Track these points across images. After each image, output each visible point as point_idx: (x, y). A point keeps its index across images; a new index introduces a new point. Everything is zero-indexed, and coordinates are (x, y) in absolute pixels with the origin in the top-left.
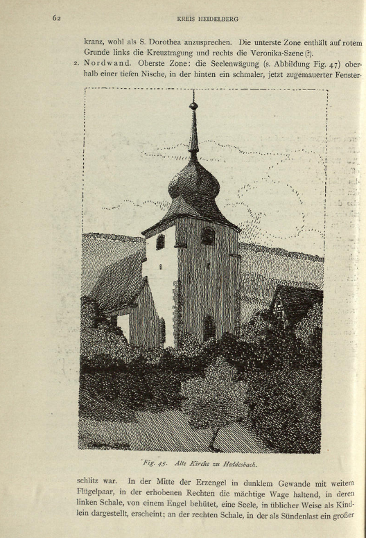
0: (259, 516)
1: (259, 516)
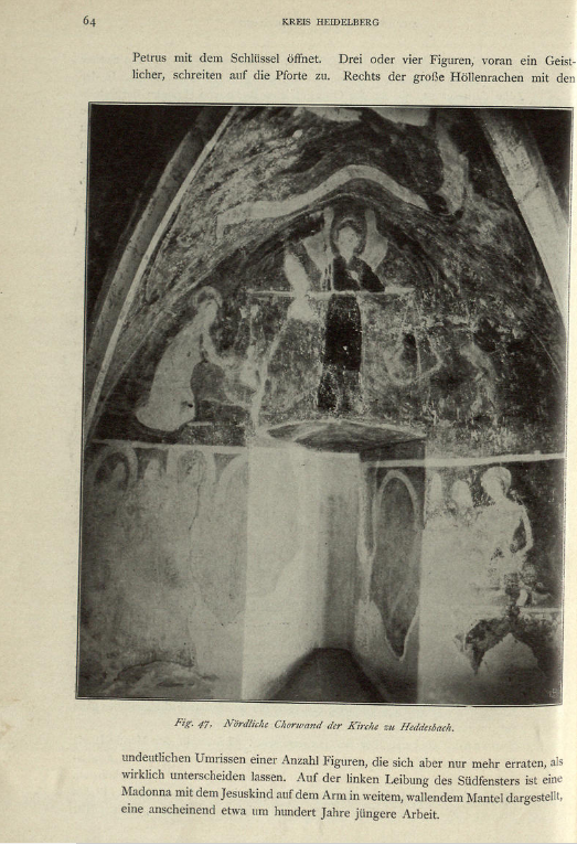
0: (438, 781)
1: (438, 781)
